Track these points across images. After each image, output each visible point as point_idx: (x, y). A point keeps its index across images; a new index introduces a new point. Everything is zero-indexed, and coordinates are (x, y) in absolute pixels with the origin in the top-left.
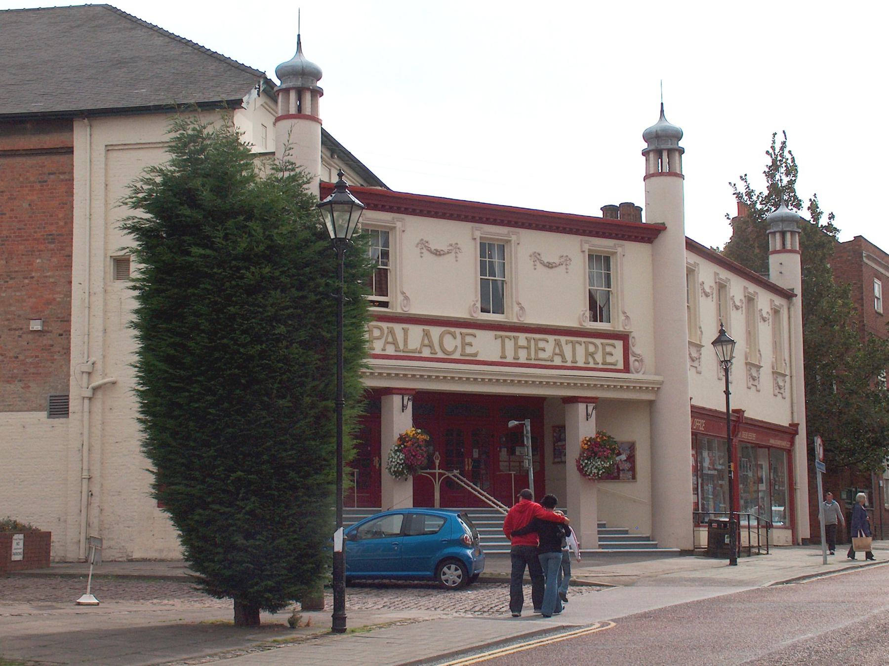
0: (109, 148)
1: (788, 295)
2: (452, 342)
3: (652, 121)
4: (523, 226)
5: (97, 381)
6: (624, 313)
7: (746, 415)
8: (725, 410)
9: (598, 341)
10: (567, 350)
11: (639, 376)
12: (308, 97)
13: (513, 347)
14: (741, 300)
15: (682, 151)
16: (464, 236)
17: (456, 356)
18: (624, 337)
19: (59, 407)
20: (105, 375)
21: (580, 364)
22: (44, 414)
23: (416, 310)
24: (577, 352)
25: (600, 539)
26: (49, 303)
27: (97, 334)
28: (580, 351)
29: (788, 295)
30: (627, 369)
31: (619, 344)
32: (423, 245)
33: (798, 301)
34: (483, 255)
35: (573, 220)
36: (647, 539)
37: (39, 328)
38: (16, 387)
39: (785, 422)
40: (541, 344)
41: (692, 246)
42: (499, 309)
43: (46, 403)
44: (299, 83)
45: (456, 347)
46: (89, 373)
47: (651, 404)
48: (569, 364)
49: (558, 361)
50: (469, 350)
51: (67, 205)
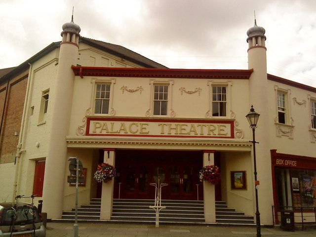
2: (136, 128)
4: (175, 77)
6: (292, 118)
7: (277, 152)
9: (216, 125)
11: (240, 140)
12: (260, 39)
13: (166, 129)
16: (205, 86)
17: (138, 134)
18: (231, 122)
21: (205, 135)
23: (118, 115)
24: (205, 129)
30: (233, 136)
31: (228, 126)
32: (124, 89)
35: (181, 71)
41: (271, 78)
42: (164, 113)
44: (72, 31)
45: (138, 130)
48: (199, 135)
49: (192, 134)
50: (144, 131)
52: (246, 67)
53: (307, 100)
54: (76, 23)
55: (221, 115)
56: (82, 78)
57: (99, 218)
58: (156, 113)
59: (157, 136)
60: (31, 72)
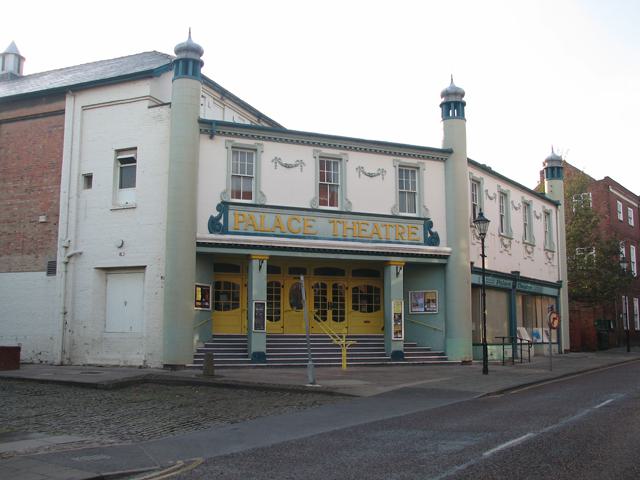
0: (85, 108)
1: (556, 204)
3: (446, 85)
5: (70, 252)
7: (521, 275)
8: (481, 267)
10: (383, 231)
14: (495, 194)
15: (464, 104)
19: (51, 269)
20: (76, 247)
21: (349, 237)
22: (45, 273)
25: (383, 345)
26: (50, 204)
27: (72, 223)
28: (392, 231)
29: (556, 204)
33: (562, 208)
34: (322, 167)
36: (304, 337)
37: (43, 220)
38: (31, 257)
39: (553, 279)
40: (365, 227)
41: (472, 163)
43: (46, 266)
46: (66, 248)
47: (444, 266)
51: (61, 145)
52: (439, 145)
53: (497, 194)
54: (197, 40)
55: (331, 205)
56: (211, 137)
57: (446, 359)
58: (402, 209)
59: (326, 236)
60: (72, 105)
